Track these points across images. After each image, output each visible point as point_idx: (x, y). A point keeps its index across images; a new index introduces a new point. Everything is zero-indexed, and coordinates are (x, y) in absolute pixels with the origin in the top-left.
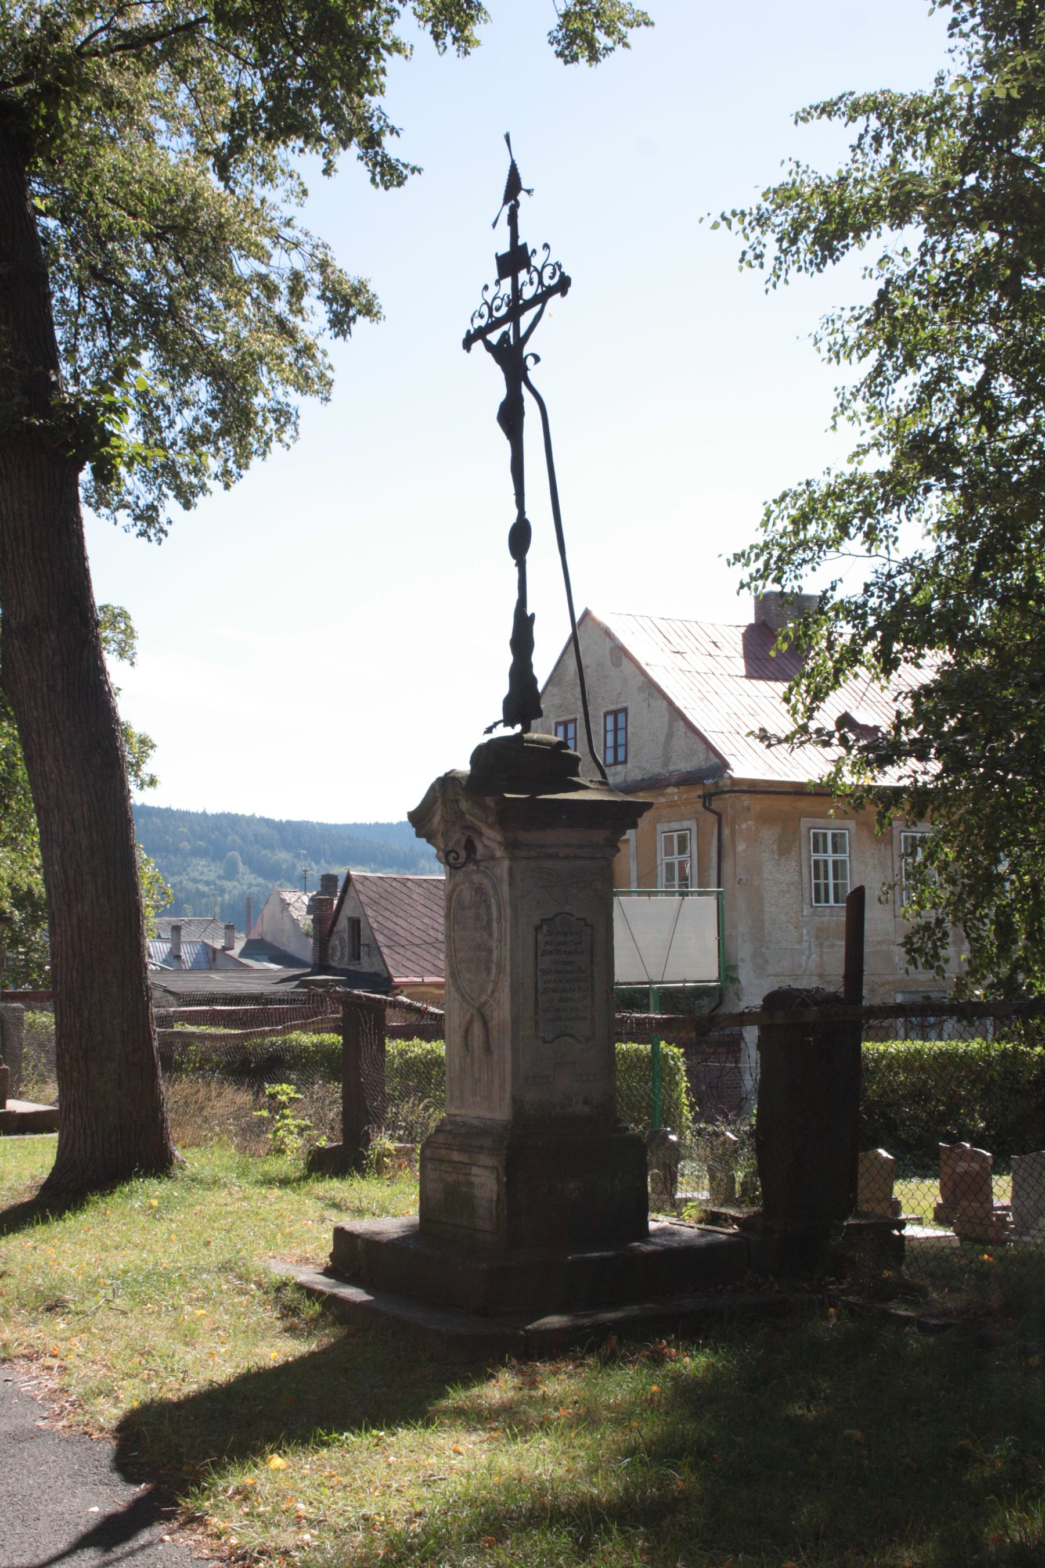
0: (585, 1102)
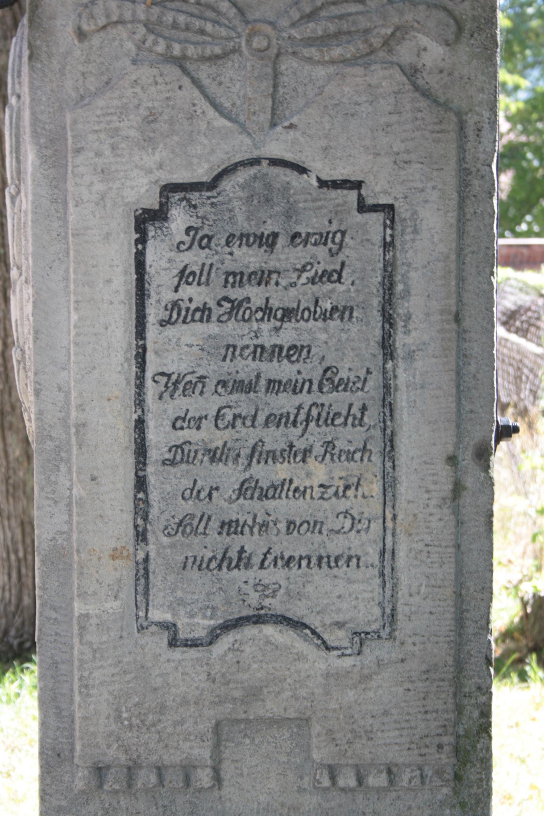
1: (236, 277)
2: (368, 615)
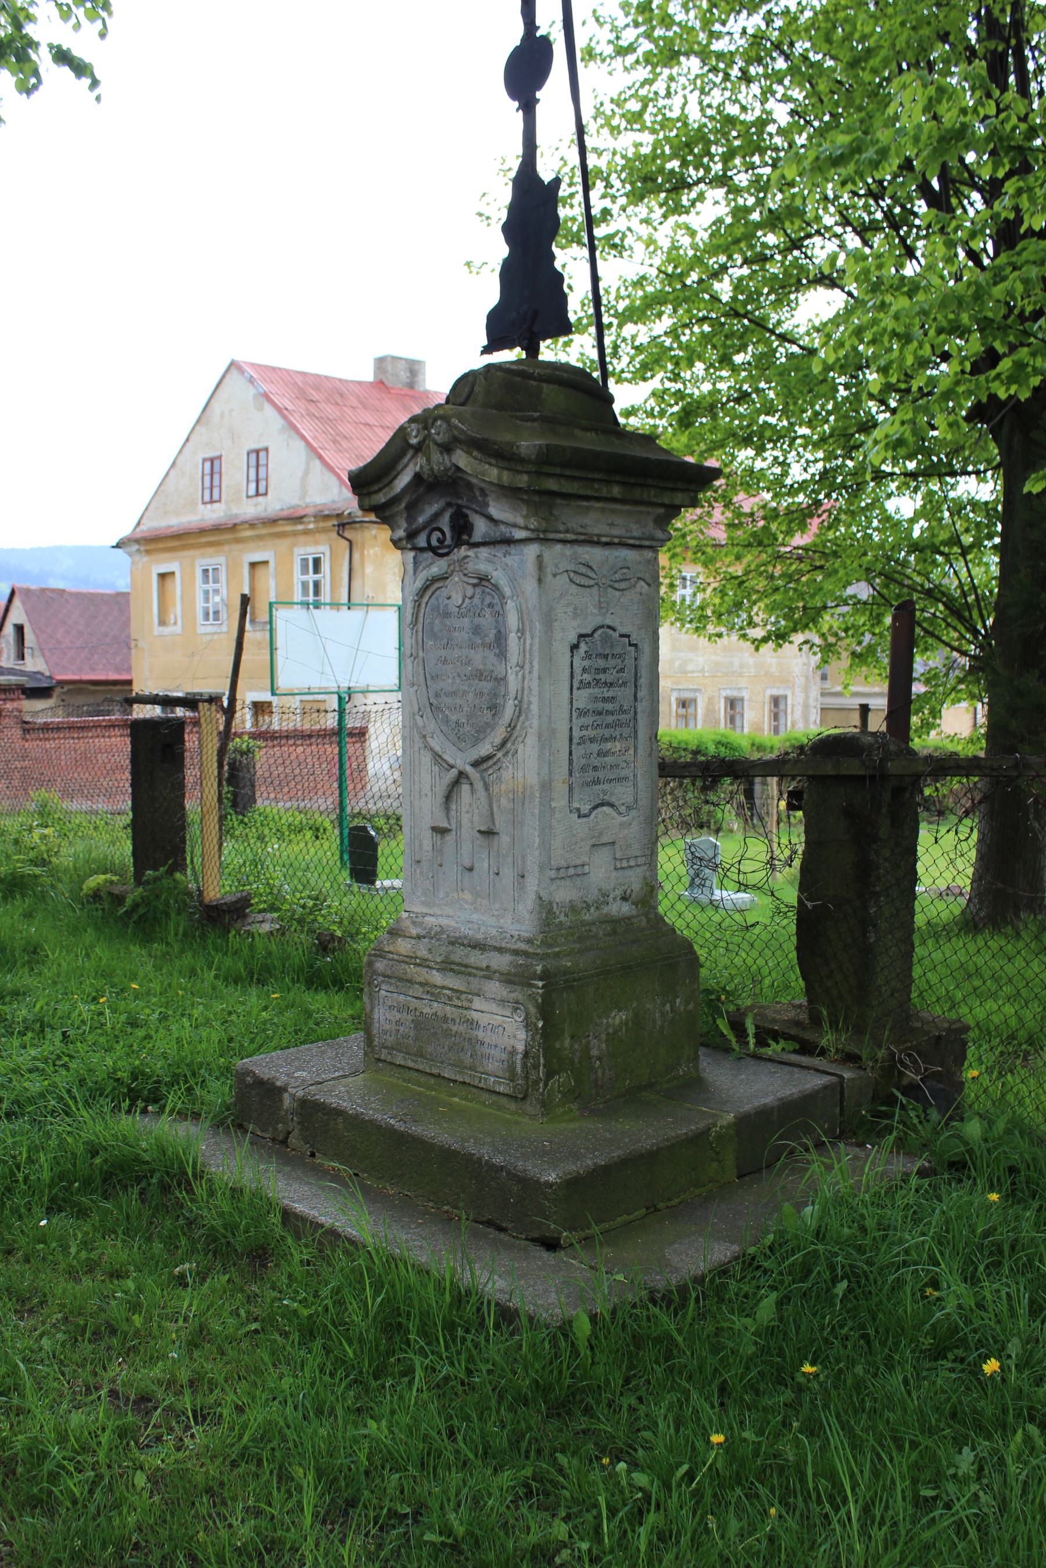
0: (624, 899)
1: (598, 671)
2: (630, 799)
